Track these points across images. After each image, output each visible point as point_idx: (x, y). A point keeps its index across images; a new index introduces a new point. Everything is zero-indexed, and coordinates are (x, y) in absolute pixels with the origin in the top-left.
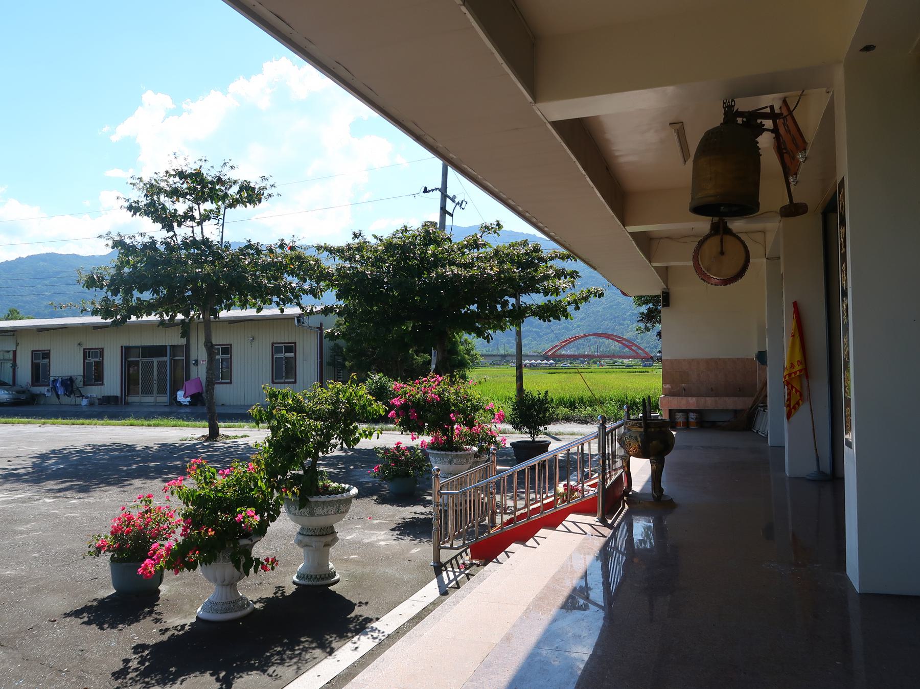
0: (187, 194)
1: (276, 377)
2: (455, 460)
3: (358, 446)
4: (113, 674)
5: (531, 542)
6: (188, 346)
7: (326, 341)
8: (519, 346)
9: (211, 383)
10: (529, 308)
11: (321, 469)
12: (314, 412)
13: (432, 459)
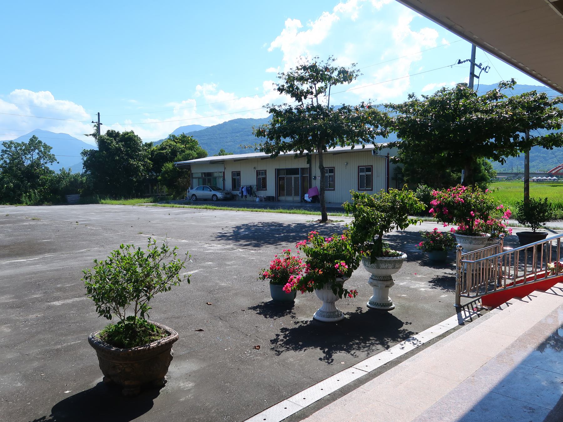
0: (308, 79)
1: (361, 187)
2: (474, 242)
3: (408, 229)
4: (271, 341)
5: (526, 298)
6: (310, 168)
7: (391, 164)
8: (527, 167)
9: (323, 189)
10: (536, 139)
11: (385, 242)
12: (380, 207)
13: (458, 240)
